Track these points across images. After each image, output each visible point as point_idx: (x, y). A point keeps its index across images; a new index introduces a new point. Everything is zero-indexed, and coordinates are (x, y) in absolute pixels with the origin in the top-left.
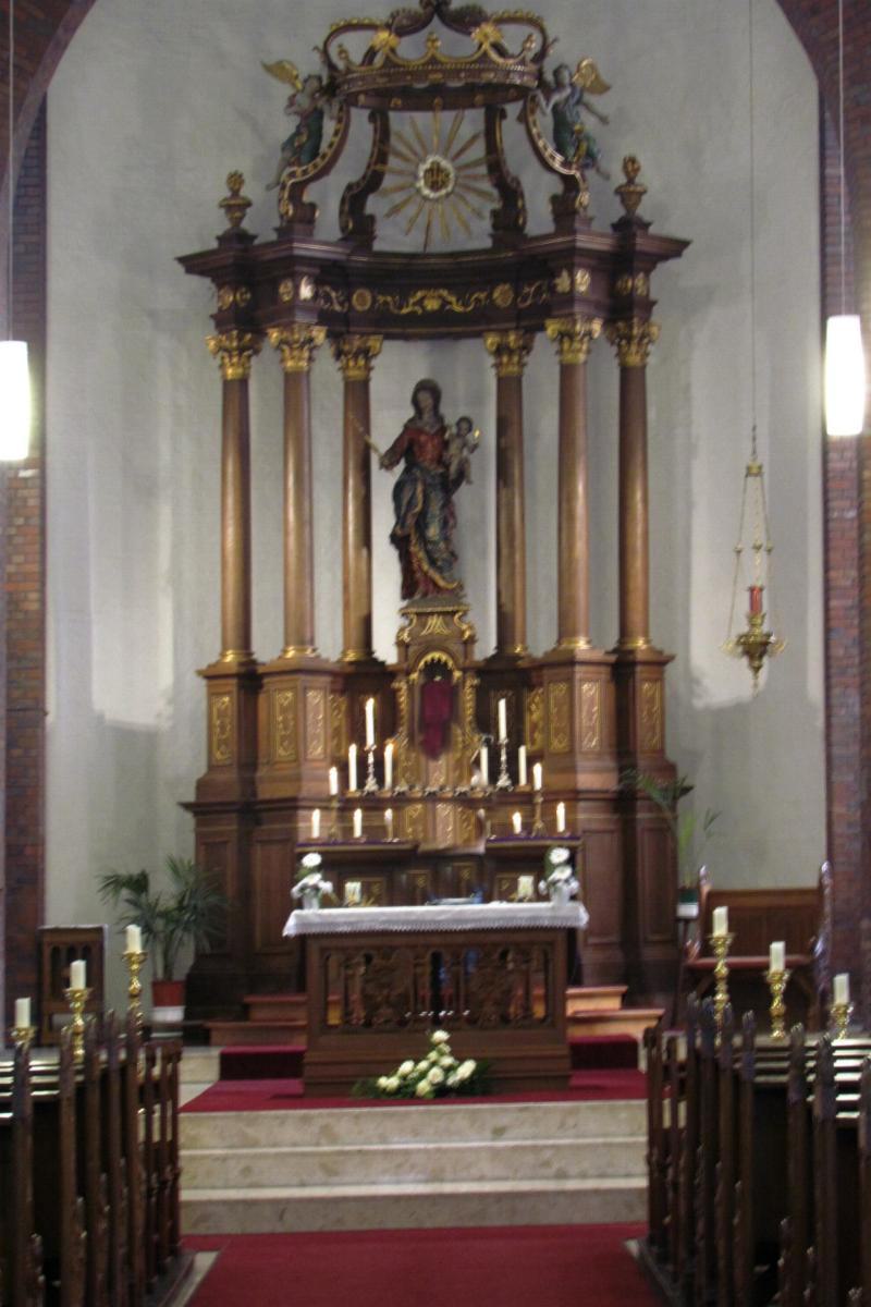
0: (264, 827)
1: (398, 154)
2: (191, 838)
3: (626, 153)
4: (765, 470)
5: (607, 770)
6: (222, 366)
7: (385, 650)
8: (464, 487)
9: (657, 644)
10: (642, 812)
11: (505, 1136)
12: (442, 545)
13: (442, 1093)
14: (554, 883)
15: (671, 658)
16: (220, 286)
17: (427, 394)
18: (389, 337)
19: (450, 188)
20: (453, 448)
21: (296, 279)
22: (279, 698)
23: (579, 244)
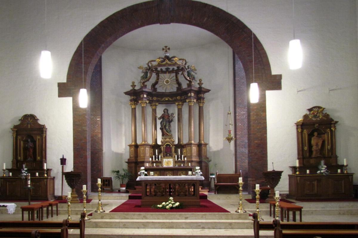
0: (139, 165)
1: (161, 79)
2: (127, 166)
3: (200, 78)
4: (231, 113)
5: (197, 158)
6: (131, 106)
7: (159, 143)
8: (172, 122)
9: (205, 142)
10: (203, 162)
11: (188, 219)
12: (169, 129)
13: (172, 209)
14: (197, 173)
15: (208, 144)
16: (131, 96)
17: (166, 111)
18: (159, 104)
19: (170, 83)
20: (170, 117)
21: (143, 94)
22: (141, 149)
23: (192, 89)
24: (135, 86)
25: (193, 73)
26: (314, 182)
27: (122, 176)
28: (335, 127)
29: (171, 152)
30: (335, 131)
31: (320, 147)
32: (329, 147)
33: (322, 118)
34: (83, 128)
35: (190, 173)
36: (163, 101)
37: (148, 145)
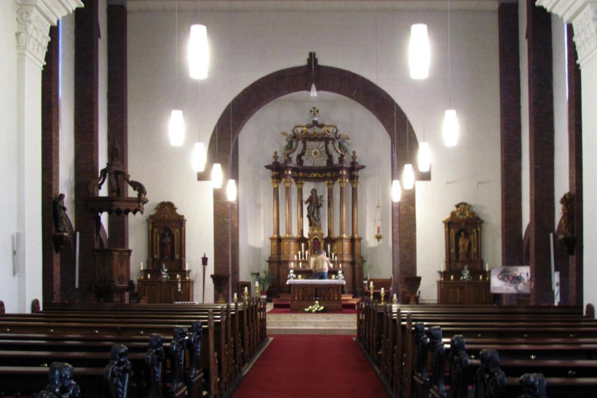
1: (308, 149)
7: (306, 235)
13: (317, 312)
17: (314, 191)
20: (319, 201)
24: (278, 157)
25: (345, 144)
26: (456, 290)
27: (263, 280)
28: (481, 227)
29: (319, 248)
30: (481, 231)
31: (466, 249)
32: (475, 250)
33: (468, 216)
34: (225, 219)
35: (333, 276)
36: (311, 178)
37: (292, 239)
